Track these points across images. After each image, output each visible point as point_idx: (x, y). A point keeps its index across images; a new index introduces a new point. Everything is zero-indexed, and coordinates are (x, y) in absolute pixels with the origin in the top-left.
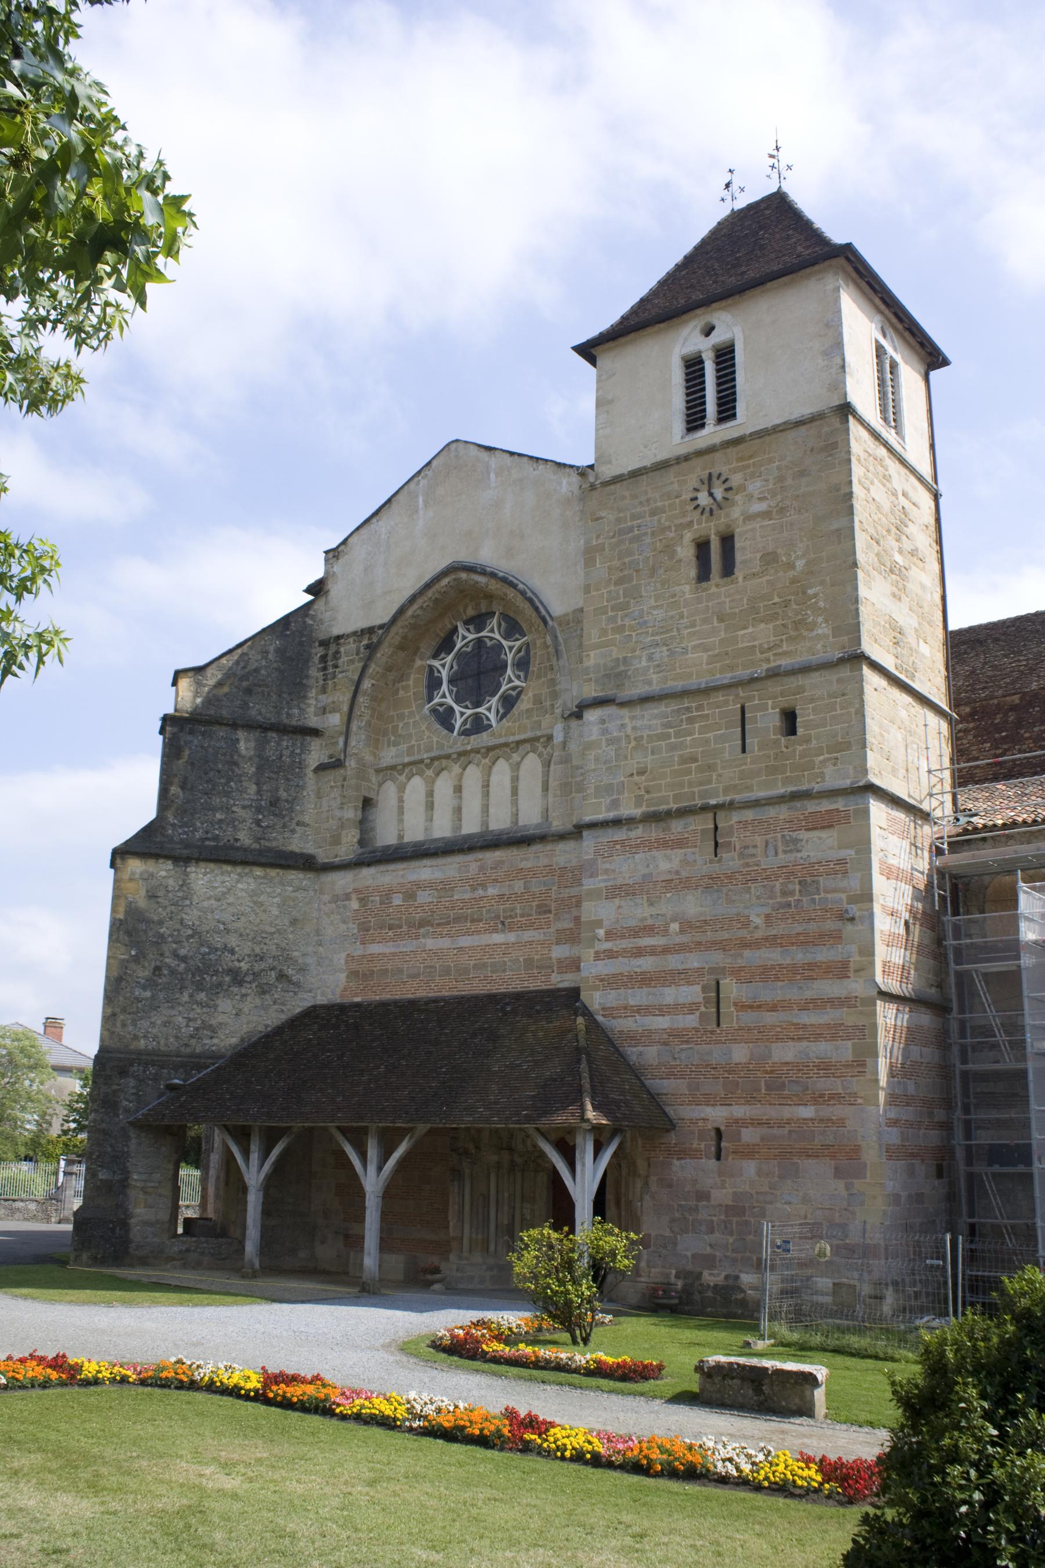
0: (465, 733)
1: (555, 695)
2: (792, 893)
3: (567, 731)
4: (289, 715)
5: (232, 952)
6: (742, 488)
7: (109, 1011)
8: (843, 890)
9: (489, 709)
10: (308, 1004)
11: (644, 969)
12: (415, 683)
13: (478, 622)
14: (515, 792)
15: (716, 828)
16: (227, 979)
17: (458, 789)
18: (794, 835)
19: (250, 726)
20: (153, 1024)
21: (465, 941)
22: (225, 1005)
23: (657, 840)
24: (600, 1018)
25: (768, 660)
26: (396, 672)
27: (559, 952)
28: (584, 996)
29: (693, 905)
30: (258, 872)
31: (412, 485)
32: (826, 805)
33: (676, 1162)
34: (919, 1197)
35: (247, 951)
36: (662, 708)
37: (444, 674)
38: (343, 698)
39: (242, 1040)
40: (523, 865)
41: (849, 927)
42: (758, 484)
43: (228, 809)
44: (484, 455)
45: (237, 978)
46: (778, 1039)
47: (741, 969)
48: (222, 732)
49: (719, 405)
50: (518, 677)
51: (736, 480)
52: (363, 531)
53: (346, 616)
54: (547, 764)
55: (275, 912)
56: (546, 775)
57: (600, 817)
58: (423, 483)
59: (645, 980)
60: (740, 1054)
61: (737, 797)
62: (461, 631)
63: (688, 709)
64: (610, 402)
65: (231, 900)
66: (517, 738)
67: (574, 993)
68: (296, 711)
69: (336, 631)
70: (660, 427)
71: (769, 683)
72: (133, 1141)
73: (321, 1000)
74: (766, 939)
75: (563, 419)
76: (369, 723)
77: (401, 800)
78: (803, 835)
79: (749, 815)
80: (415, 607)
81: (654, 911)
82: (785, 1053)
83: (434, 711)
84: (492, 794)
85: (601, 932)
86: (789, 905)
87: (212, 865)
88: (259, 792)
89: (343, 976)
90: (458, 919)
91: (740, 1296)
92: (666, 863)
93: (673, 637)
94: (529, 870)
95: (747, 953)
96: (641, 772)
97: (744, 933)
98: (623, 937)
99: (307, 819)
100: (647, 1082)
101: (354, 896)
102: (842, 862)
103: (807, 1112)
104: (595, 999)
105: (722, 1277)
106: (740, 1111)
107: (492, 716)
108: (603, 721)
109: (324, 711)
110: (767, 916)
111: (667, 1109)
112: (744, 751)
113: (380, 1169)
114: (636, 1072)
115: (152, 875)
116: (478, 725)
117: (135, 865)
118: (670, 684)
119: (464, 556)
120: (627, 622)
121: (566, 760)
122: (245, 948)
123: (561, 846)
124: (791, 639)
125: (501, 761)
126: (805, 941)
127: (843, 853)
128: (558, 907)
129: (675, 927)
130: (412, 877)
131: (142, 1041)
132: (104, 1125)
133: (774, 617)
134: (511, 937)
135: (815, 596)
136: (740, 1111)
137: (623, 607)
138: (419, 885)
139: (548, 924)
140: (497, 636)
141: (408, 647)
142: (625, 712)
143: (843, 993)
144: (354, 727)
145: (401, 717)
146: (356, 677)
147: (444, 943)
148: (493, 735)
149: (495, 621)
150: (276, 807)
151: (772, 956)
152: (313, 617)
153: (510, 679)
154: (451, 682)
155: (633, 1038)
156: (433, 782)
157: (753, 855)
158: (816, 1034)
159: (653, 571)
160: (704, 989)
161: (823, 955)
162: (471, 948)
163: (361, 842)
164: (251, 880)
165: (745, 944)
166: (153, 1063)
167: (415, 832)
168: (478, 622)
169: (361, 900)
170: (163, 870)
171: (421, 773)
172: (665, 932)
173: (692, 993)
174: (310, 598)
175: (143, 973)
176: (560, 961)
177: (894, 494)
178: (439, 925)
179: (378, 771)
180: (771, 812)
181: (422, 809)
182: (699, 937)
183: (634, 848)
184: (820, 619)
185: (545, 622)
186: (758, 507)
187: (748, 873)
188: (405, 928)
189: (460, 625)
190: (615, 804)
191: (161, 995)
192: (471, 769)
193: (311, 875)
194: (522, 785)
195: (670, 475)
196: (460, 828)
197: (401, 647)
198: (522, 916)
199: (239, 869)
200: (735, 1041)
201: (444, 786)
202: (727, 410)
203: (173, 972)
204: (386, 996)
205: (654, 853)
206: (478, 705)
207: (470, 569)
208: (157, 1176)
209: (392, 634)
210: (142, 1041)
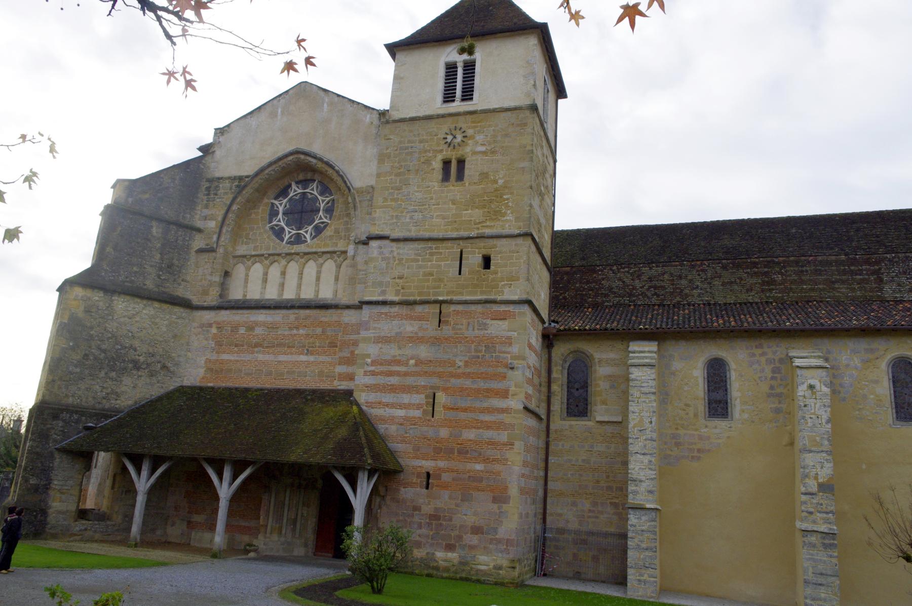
0: (289, 243)
1: (348, 230)
2: (481, 351)
4: (184, 217)
5: (135, 350)
6: (472, 137)
7: (51, 378)
8: (508, 353)
9: (306, 232)
11: (392, 382)
12: (262, 211)
13: (305, 183)
14: (318, 279)
15: (440, 312)
16: (130, 365)
17: (283, 273)
20: (79, 389)
21: (282, 358)
22: (127, 381)
23: (406, 315)
24: (364, 408)
25: (478, 229)
26: (251, 204)
27: (340, 369)
28: (356, 395)
29: (424, 352)
30: (156, 305)
31: (275, 102)
32: (503, 308)
33: (403, 489)
34: (527, 515)
35: (145, 350)
36: (416, 245)
37: (281, 209)
39: (136, 403)
40: (323, 319)
41: (510, 372)
44: (322, 93)
45: (137, 366)
47: (448, 388)
49: (463, 92)
50: (326, 217)
51: (470, 132)
52: (241, 121)
53: (226, 166)
55: (164, 329)
56: (338, 272)
57: (374, 298)
58: (282, 101)
59: (393, 389)
60: (444, 433)
61: (455, 298)
62: (294, 186)
63: (431, 248)
64: (402, 78)
65: (138, 319)
66: (323, 250)
67: (349, 393)
68: (188, 216)
69: (217, 175)
70: (429, 97)
71: (477, 240)
72: (57, 460)
73: (187, 382)
74: (464, 374)
75: (371, 83)
76: (233, 229)
77: (247, 275)
78: (489, 321)
79: (460, 308)
80: (270, 169)
82: (470, 435)
83: (272, 228)
84: (304, 279)
85: (369, 361)
86: (478, 357)
87: (128, 298)
88: (162, 259)
89: (202, 371)
90: (280, 345)
91: (435, 564)
92: (410, 327)
93: (426, 209)
94: (326, 322)
95: (453, 380)
98: (381, 364)
99: (188, 278)
100: (389, 445)
101: (214, 326)
102: (509, 338)
103: (479, 467)
104: (362, 397)
105: (424, 554)
107: (308, 236)
109: (206, 218)
110: (466, 362)
111: (400, 460)
112: (460, 274)
114: (383, 439)
115: (89, 299)
116: (298, 240)
117: (79, 291)
118: (421, 233)
120: (400, 196)
121: (354, 266)
124: (491, 219)
126: (486, 377)
127: (510, 334)
129: (412, 362)
130: (253, 318)
131: (71, 399)
132: (38, 450)
133: (484, 207)
134: (311, 358)
135: (507, 199)
136: (441, 464)
137: (399, 189)
138: (257, 324)
139: (335, 353)
140: (315, 193)
141: (262, 191)
142: (394, 244)
144: (224, 230)
146: (228, 203)
147: (267, 357)
148: (308, 246)
149: (315, 185)
150: (171, 269)
151: (468, 383)
152: (204, 165)
153: (321, 217)
154: (284, 214)
155: (383, 420)
156: (268, 268)
157: (460, 329)
158: (488, 426)
160: (427, 397)
161: (494, 385)
162: (286, 362)
163: (221, 296)
164: (151, 309)
165: (453, 375)
166: (76, 412)
167: (254, 293)
168: (305, 183)
169: (218, 328)
170: (97, 297)
171: (261, 262)
172: (407, 364)
174: (200, 154)
176: (340, 374)
178: (267, 347)
179: (235, 257)
180: (473, 308)
181: (260, 282)
182: (426, 369)
185: (349, 190)
187: (457, 338)
188: (245, 347)
190: (383, 293)
191: (87, 372)
192: (292, 264)
193: (188, 311)
194: (323, 275)
195: (432, 124)
196: (282, 295)
197: (257, 190)
198: (319, 347)
199: (145, 302)
200: (442, 426)
201: (275, 271)
202: (468, 95)
203: (95, 358)
204: (230, 384)
205: (404, 322)
206: (300, 229)
208: (71, 482)
209: (254, 182)
210: (71, 399)
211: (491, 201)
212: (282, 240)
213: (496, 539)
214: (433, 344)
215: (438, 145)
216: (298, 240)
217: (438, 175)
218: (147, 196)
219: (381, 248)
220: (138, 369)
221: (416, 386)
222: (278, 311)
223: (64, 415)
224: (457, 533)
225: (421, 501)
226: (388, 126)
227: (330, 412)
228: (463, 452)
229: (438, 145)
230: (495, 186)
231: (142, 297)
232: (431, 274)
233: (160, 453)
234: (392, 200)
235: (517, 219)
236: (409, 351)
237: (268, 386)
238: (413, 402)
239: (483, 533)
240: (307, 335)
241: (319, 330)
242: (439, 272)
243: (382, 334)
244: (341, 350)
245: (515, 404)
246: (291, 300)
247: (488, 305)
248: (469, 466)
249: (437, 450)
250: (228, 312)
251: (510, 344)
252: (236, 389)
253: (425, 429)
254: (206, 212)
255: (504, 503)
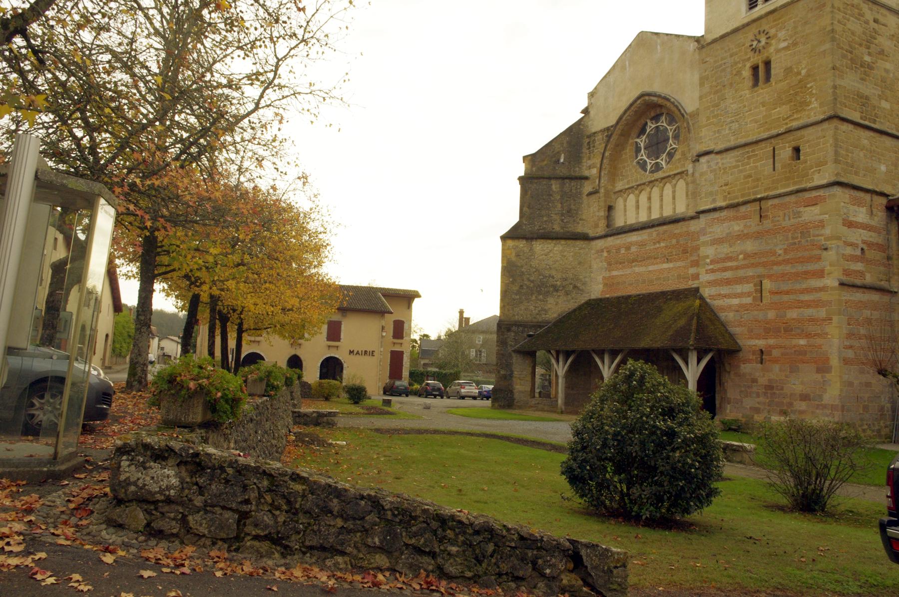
0: (652, 172)
2: (797, 238)
3: (694, 168)
5: (553, 277)
8: (821, 235)
10: (587, 299)
12: (629, 151)
14: (674, 198)
17: (649, 199)
18: (798, 209)
19: (556, 178)
21: (651, 268)
22: (551, 300)
24: (708, 300)
25: (786, 124)
26: (619, 147)
27: (692, 271)
28: (701, 290)
29: (750, 246)
30: (563, 242)
31: (611, 79)
32: (814, 194)
33: (742, 365)
38: (597, 161)
40: (676, 232)
41: (825, 253)
42: (783, 32)
43: (549, 216)
44: (655, 37)
45: (556, 289)
46: (790, 308)
47: (772, 275)
48: (545, 182)
51: (772, 32)
53: (599, 123)
54: (687, 184)
57: (707, 207)
60: (771, 315)
62: (649, 124)
63: (748, 152)
67: (697, 290)
69: (593, 131)
71: (787, 135)
73: (593, 297)
74: (784, 261)
76: (609, 172)
77: (625, 206)
78: (802, 209)
79: (776, 201)
81: (732, 249)
82: (792, 314)
85: (708, 261)
86: (795, 243)
88: (562, 207)
89: (601, 286)
90: (649, 258)
92: (737, 227)
95: (775, 267)
96: (726, 185)
97: (773, 258)
98: (718, 262)
99: (584, 217)
102: (822, 221)
103: (802, 342)
104: (706, 292)
106: (771, 342)
107: (663, 163)
108: (708, 162)
109: (590, 168)
110: (785, 249)
111: (738, 341)
113: (610, 368)
117: (510, 243)
119: (647, 89)
121: (694, 182)
122: (558, 276)
123: (692, 222)
124: (798, 112)
125: (668, 184)
127: (821, 217)
128: (687, 251)
129: (741, 256)
134: (671, 265)
135: (811, 87)
136: (771, 342)
137: (717, 105)
138: (631, 244)
139: (687, 258)
140: (665, 124)
142: (718, 156)
143: (821, 285)
144: (602, 174)
145: (624, 167)
150: (571, 213)
151: (788, 268)
152: (583, 125)
153: (672, 144)
154: (645, 148)
155: (723, 309)
158: (808, 305)
159: (731, 84)
160: (755, 285)
161: (811, 267)
163: (608, 226)
166: (521, 325)
167: (631, 220)
168: (656, 118)
170: (522, 244)
173: (748, 287)
175: (515, 288)
176: (692, 275)
177: (867, 22)
179: (615, 193)
180: (787, 199)
181: (634, 209)
183: (721, 221)
184: (813, 99)
185: (683, 116)
186: (783, 45)
189: (648, 121)
193: (586, 242)
194: (677, 194)
199: (554, 241)
201: (643, 197)
203: (528, 287)
204: (619, 294)
205: (732, 223)
206: (657, 158)
207: (649, 95)
211: (796, 94)
212: (645, 171)
213: (822, 405)
214: (757, 238)
215: (746, 53)
216: (657, 167)
217: (749, 83)
218: (545, 162)
219: (708, 162)
220: (557, 291)
221: (746, 277)
222: (644, 231)
223: (514, 328)
224: (788, 400)
225: (757, 374)
226: (704, 50)
227: (679, 307)
228: (788, 330)
229: (746, 53)
230: (799, 77)
231: (552, 239)
232: (750, 176)
233: (568, 349)
234: (714, 117)
235: (821, 105)
236: (739, 247)
237: (644, 292)
238: (745, 291)
239: (810, 400)
240: (666, 247)
241: (674, 241)
242: (761, 172)
243: (716, 237)
244: (691, 255)
245: (831, 282)
246: (658, 219)
247: (800, 194)
248: (795, 342)
249: (767, 331)
250: (612, 238)
251: (823, 227)
252: (623, 297)
253: (756, 312)
254: (590, 162)
255: (827, 373)
